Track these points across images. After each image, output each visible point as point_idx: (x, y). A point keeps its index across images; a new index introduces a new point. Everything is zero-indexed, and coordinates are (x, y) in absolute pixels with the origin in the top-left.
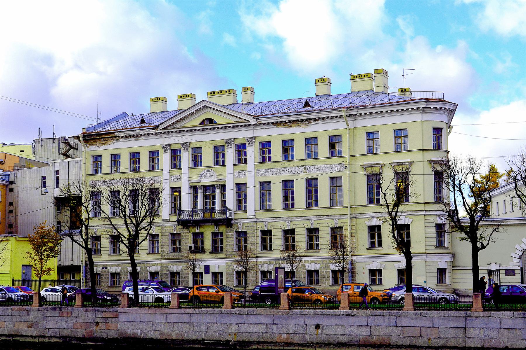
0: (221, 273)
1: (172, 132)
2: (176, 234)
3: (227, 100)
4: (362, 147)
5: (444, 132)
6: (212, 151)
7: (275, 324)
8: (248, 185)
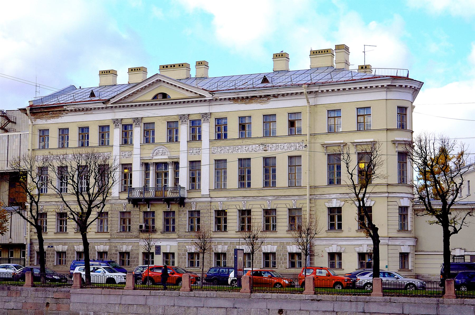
0: (173, 254)
1: (124, 106)
2: (126, 212)
3: (180, 74)
4: (322, 126)
5: (408, 111)
6: (165, 126)
7: (236, 308)
8: (202, 163)
